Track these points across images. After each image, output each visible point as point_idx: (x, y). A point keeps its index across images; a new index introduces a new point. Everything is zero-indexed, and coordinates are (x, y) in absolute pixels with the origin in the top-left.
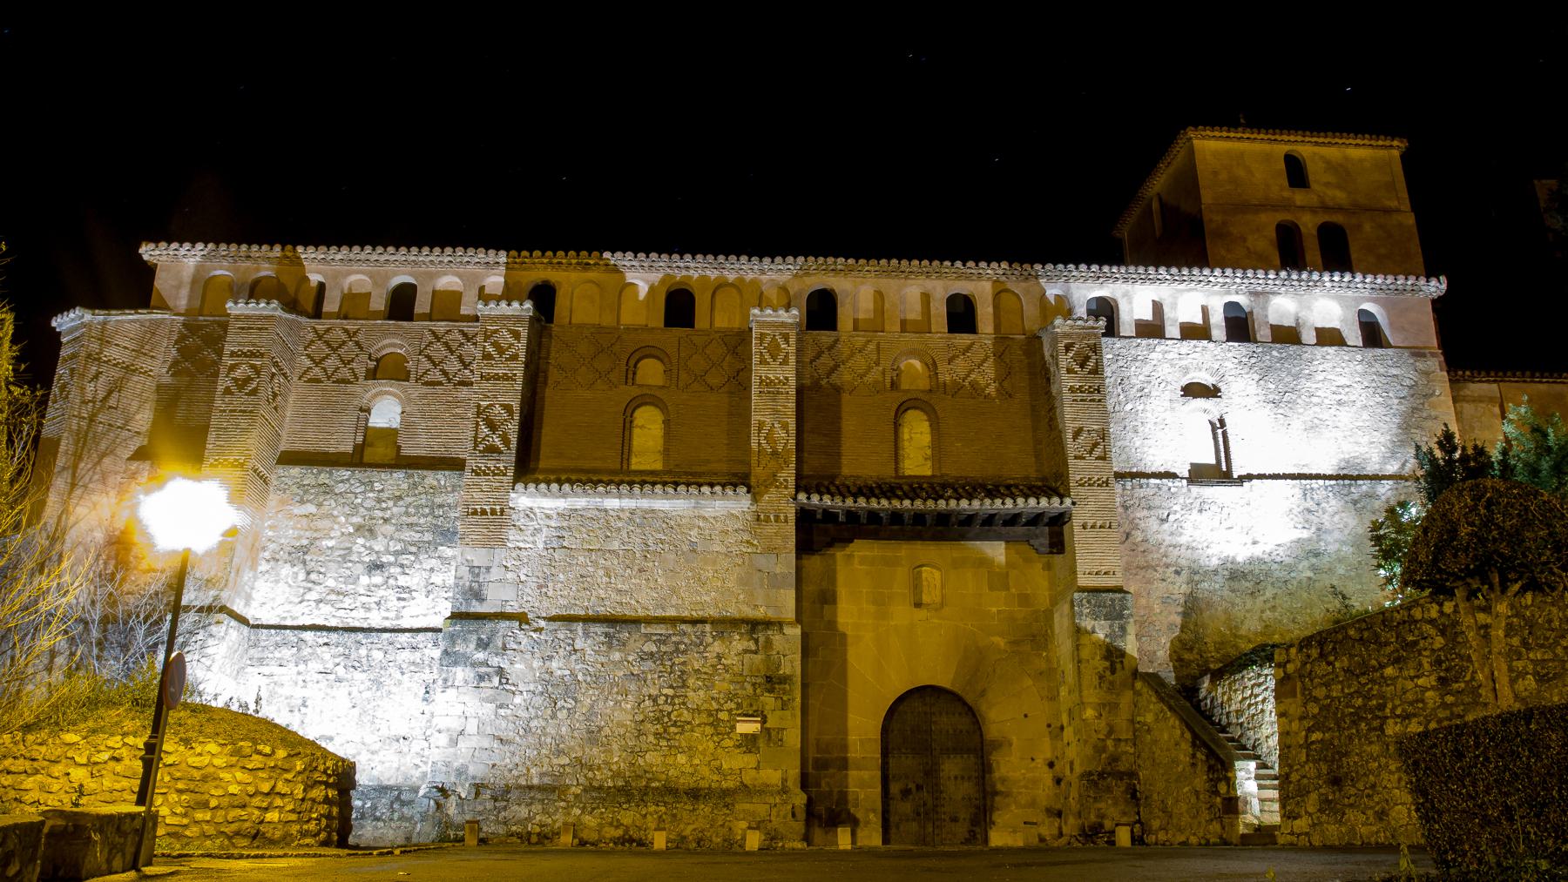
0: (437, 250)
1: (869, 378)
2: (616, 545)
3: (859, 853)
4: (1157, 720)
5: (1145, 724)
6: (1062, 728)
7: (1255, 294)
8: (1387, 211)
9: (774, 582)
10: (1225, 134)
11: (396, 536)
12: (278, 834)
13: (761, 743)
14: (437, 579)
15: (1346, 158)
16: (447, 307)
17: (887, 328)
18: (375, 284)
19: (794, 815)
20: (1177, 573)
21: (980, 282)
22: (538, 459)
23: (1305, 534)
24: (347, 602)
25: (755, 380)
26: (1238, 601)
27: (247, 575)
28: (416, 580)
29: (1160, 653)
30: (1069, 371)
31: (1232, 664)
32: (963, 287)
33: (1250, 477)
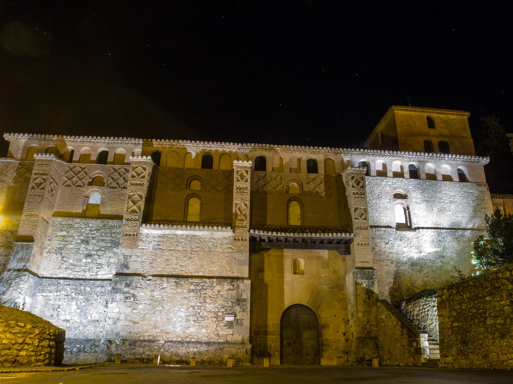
0: (116, 138)
1: (278, 189)
2: (180, 248)
3: (272, 368)
4: (386, 317)
5: (381, 319)
6: (349, 320)
7: (420, 162)
8: (463, 137)
9: (241, 263)
10: (406, 109)
11: (97, 244)
12: (25, 361)
13: (234, 324)
14: (112, 261)
15: (448, 119)
16: (120, 159)
17: (285, 171)
18: (93, 150)
19: (246, 352)
20: (392, 263)
21: (320, 154)
22: (152, 216)
23: (439, 250)
24: (77, 269)
25: (235, 187)
26: (414, 274)
27: (38, 258)
28: (104, 261)
29: (385, 293)
30: (353, 187)
31: (413, 297)
32: (313, 156)
33: (418, 228)
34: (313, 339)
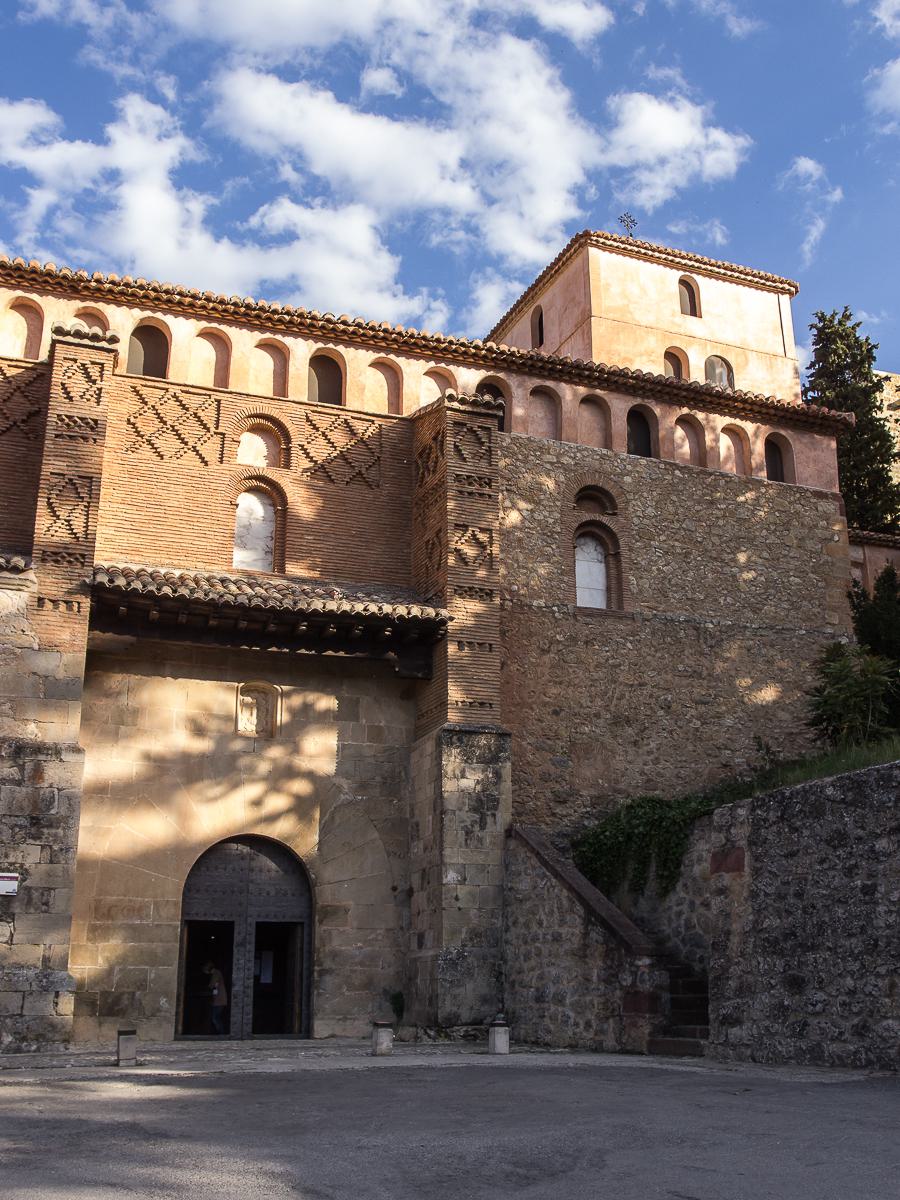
6: (410, 892)
13: (17, 908)
34: (261, 871)
